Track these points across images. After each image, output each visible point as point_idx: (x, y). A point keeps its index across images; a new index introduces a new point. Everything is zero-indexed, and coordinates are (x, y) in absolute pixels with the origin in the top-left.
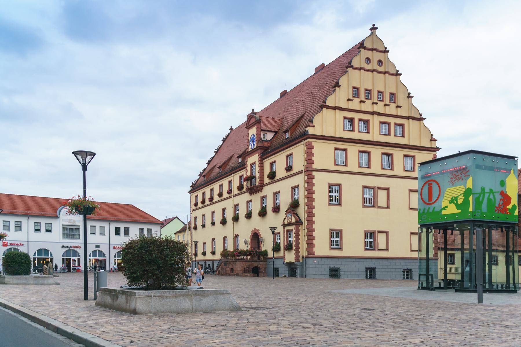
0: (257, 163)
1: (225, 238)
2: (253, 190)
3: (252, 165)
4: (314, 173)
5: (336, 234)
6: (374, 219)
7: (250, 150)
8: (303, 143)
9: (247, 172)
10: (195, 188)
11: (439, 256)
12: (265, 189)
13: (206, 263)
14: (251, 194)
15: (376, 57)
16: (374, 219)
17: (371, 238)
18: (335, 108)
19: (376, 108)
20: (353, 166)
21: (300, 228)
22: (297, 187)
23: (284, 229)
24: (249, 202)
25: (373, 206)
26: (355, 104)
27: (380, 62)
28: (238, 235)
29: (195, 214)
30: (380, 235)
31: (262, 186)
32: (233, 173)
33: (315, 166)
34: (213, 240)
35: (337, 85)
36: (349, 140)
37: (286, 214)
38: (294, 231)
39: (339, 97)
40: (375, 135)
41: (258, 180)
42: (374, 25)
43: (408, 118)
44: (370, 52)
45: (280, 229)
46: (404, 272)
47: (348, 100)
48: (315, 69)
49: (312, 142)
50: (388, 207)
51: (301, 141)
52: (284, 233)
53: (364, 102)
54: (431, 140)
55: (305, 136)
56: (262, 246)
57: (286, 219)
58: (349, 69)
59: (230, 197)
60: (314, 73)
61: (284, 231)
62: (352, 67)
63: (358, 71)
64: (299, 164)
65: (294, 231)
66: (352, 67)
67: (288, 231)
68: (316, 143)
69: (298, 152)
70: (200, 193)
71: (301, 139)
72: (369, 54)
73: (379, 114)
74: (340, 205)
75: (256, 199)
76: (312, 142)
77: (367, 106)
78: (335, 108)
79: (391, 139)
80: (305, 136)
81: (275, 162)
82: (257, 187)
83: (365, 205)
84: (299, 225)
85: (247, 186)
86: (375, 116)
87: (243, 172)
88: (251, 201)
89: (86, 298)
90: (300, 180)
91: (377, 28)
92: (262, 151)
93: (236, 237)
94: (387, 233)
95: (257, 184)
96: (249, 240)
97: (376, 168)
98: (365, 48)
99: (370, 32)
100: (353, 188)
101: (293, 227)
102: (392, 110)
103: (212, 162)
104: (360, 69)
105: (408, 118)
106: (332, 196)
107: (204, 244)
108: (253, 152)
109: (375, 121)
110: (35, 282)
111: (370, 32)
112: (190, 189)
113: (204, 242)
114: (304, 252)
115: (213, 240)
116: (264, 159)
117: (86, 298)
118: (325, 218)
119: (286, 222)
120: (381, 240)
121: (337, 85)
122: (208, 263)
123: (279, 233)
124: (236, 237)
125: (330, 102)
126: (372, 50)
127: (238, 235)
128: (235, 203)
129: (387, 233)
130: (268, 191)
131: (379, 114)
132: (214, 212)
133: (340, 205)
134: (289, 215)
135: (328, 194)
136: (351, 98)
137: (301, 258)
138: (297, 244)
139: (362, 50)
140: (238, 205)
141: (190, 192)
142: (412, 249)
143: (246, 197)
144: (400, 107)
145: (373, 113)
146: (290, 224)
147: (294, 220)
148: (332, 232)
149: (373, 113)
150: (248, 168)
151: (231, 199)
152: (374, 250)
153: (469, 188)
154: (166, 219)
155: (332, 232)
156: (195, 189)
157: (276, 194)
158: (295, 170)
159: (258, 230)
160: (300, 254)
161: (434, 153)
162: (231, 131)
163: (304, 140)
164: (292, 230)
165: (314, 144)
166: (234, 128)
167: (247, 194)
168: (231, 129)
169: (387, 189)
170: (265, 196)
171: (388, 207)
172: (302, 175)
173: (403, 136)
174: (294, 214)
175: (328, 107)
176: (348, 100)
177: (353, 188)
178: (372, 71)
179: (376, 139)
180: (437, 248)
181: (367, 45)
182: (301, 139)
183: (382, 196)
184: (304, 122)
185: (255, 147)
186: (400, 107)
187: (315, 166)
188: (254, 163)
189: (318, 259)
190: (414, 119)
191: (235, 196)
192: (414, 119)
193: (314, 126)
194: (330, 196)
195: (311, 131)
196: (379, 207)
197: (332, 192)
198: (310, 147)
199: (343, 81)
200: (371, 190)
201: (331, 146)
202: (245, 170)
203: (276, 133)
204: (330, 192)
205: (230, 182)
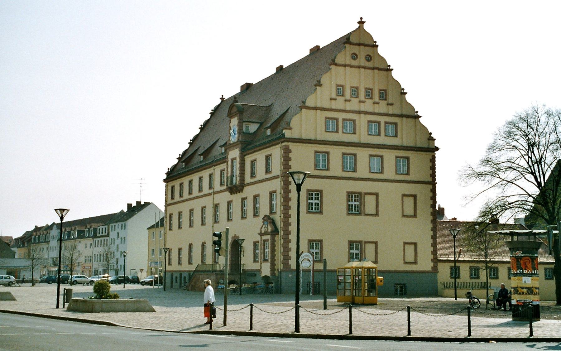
2: (234, 189)
3: (233, 160)
5: (316, 244)
6: (361, 228)
10: (172, 175)
12: (246, 189)
13: (181, 275)
15: (362, 52)
16: (361, 228)
17: (357, 248)
18: (316, 108)
19: (363, 108)
20: (336, 168)
21: (276, 238)
22: (275, 192)
24: (229, 203)
25: (360, 214)
26: (339, 104)
27: (369, 58)
30: (368, 245)
34: (190, 246)
35: (319, 84)
38: (270, 241)
39: (321, 97)
40: (363, 136)
41: (238, 179)
42: (361, 18)
43: (401, 116)
44: (357, 47)
47: (331, 99)
48: (311, 50)
49: (288, 146)
50: (377, 214)
53: (350, 101)
54: (429, 139)
55: (282, 138)
57: (263, 228)
58: (333, 67)
60: (309, 53)
63: (342, 68)
64: (277, 168)
66: (336, 65)
68: (292, 146)
69: (276, 152)
70: (177, 183)
71: (277, 142)
72: (356, 49)
73: (366, 113)
74: (321, 212)
75: (236, 198)
76: (288, 146)
77: (354, 105)
78: (316, 108)
79: (382, 140)
80: (282, 138)
84: (275, 235)
86: (362, 115)
89: (58, 307)
90: (277, 185)
91: (364, 22)
92: (244, 146)
94: (376, 243)
97: (363, 171)
98: (351, 44)
99: (358, 25)
100: (335, 195)
101: (268, 237)
103: (218, 112)
104: (345, 66)
105: (401, 116)
106: (312, 203)
107: (180, 250)
108: (234, 145)
109: (362, 121)
111: (358, 25)
112: (165, 177)
114: (279, 266)
115: (190, 246)
117: (58, 307)
118: (311, 227)
119: (263, 232)
120: (370, 250)
121: (319, 84)
125: (310, 102)
126: (359, 45)
130: (249, 192)
131: (366, 113)
133: (321, 212)
135: (307, 201)
136: (334, 96)
137: (276, 272)
138: (273, 256)
139: (347, 46)
141: (165, 181)
143: (227, 196)
144: (392, 104)
145: (359, 112)
146: (266, 234)
149: (359, 112)
153: (110, 287)
156: (170, 177)
160: (276, 267)
161: (433, 154)
162: (222, 101)
163: (282, 142)
164: (267, 240)
166: (226, 97)
167: (227, 193)
168: (222, 99)
169: (377, 195)
170: (246, 198)
171: (377, 214)
172: (279, 179)
173: (396, 136)
175: (308, 108)
176: (331, 99)
177: (335, 195)
178: (359, 67)
179: (363, 141)
181: (352, 40)
182: (277, 142)
183: (370, 202)
184: (283, 124)
186: (392, 104)
188: (235, 158)
190: (408, 117)
191: (215, 193)
192: (408, 117)
193: (291, 129)
195: (288, 134)
196: (366, 215)
197: (355, 205)
198: (287, 151)
199: (325, 80)
202: (225, 164)
203: (261, 124)
204: (309, 199)
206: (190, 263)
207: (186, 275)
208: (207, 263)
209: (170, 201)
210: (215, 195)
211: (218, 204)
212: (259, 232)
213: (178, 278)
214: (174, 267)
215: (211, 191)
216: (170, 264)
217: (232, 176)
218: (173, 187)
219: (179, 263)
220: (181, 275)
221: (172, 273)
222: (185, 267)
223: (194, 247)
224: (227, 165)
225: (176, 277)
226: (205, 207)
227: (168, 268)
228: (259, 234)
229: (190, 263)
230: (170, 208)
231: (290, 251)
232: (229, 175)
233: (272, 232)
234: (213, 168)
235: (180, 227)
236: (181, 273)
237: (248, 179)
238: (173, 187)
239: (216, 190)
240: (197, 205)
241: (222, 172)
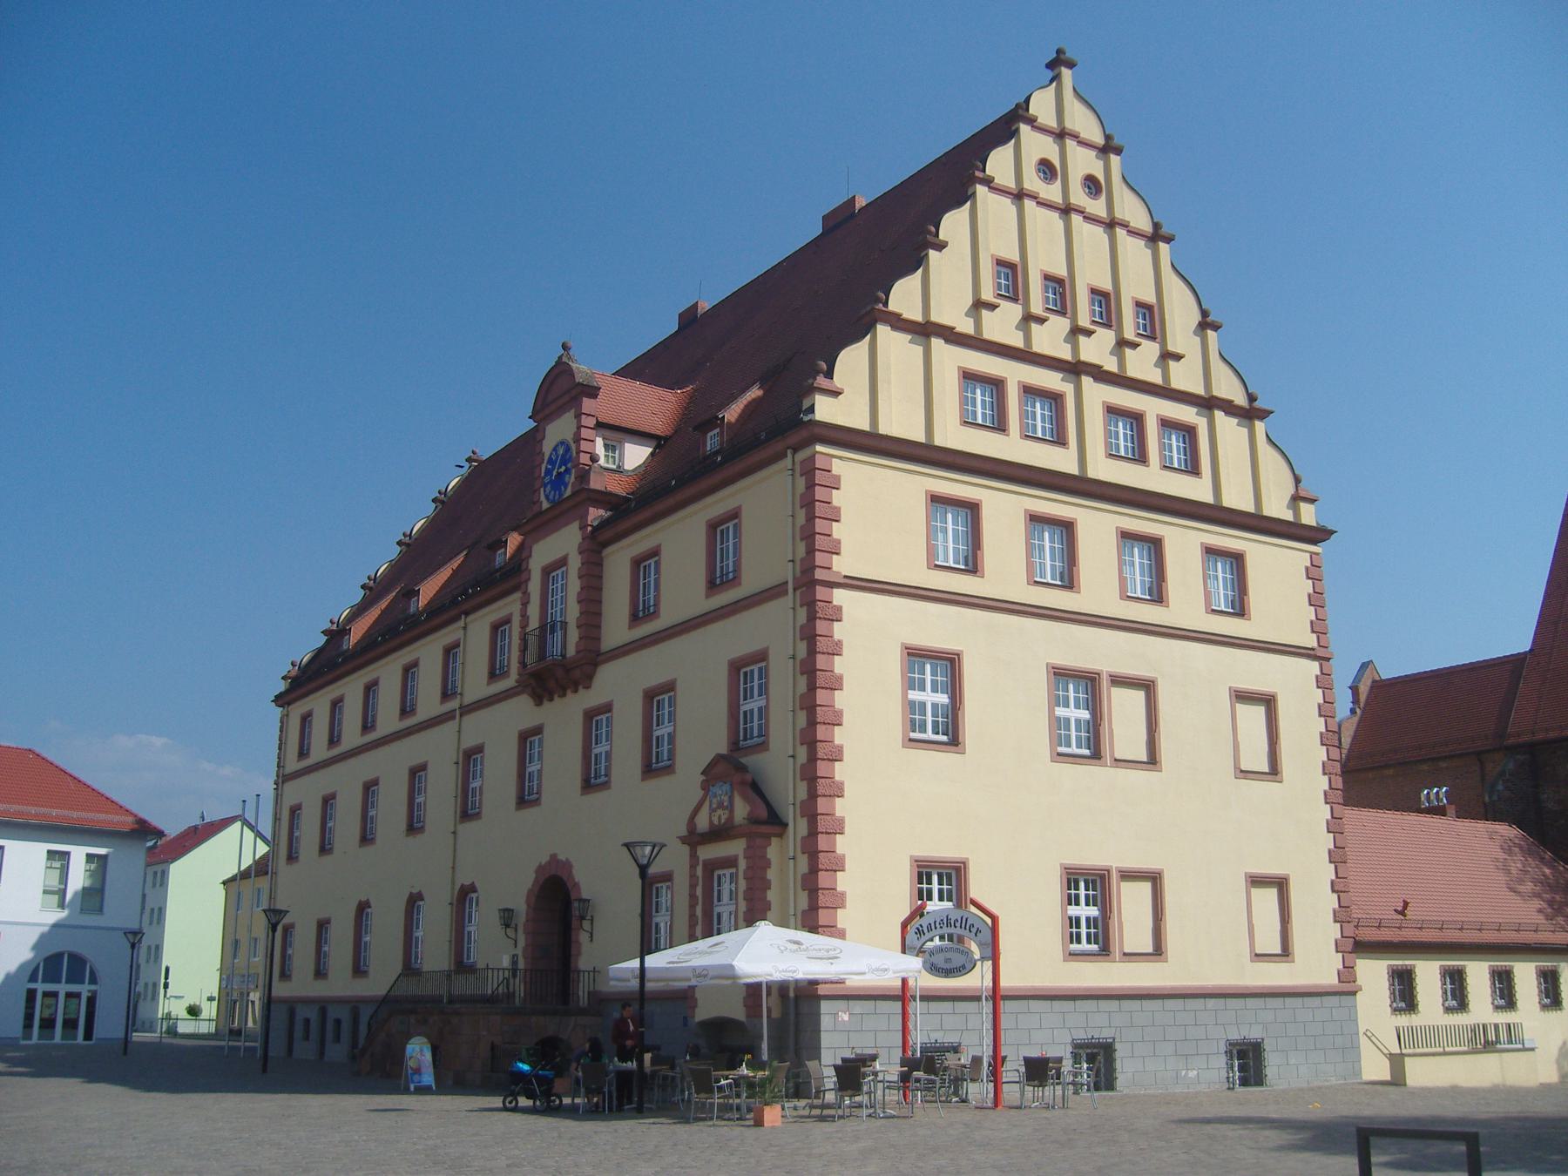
0: (575, 563)
1: (414, 901)
2: (549, 678)
3: (547, 571)
4: (840, 596)
6: (1105, 817)
7: (545, 505)
8: (788, 462)
9: (525, 604)
11: (1361, 979)
13: (323, 1012)
14: (539, 701)
21: (773, 852)
22: (762, 656)
23: (693, 856)
24: (528, 738)
25: (1096, 755)
26: (1002, 325)
28: (473, 888)
29: (293, 793)
31: (592, 658)
32: (467, 614)
33: (843, 565)
34: (363, 908)
36: (988, 467)
37: (706, 786)
38: (742, 864)
39: (944, 284)
41: (573, 635)
45: (674, 860)
46: (1229, 1054)
50: (1153, 760)
51: (783, 456)
52: (693, 876)
56: (583, 937)
57: (705, 810)
59: (447, 717)
61: (693, 867)
62: (1031, 121)
65: (742, 864)
67: (712, 866)
70: (319, 704)
75: (562, 719)
77: (1050, 338)
81: (655, 553)
82: (565, 665)
83: (1062, 749)
84: (768, 837)
85: (523, 664)
87: (509, 606)
88: (538, 730)
93: (464, 896)
94: (1155, 879)
95: (571, 651)
96: (520, 905)
100: (1009, 673)
101: (736, 848)
102: (1143, 363)
106: (923, 705)
107: (323, 926)
110: (798, 827)
112: (282, 686)
113: (322, 916)
115: (363, 908)
116: (606, 544)
119: (703, 823)
122: (333, 1013)
123: (667, 877)
124: (464, 896)
127: (473, 888)
128: (469, 742)
129: (1155, 879)
130: (618, 684)
132: (375, 782)
134: (721, 790)
140: (479, 749)
141: (280, 700)
142: (1278, 951)
143: (521, 711)
146: (718, 833)
147: (741, 810)
148: (924, 871)
150: (534, 586)
151: (451, 726)
152: (1105, 951)
154: (198, 822)
155: (924, 871)
157: (652, 697)
158: (751, 582)
159: (567, 865)
163: (795, 450)
164: (731, 862)
165: (837, 467)
166: (485, 455)
167: (524, 702)
170: (607, 708)
174: (743, 783)
177: (1009, 673)
180: (1350, 943)
183: (1125, 708)
185: (568, 492)
187: (843, 565)
188: (563, 562)
189: (858, 1007)
191: (467, 710)
193: (836, 393)
194: (912, 704)
195: (825, 410)
196: (1118, 762)
200: (1083, 683)
201: (921, 482)
202: (517, 595)
205: (450, 651)
206: (359, 970)
207: (302, 1013)
208: (425, 969)
209: (293, 765)
210: (466, 718)
211: (479, 749)
212: (683, 831)
213: (314, 1026)
214: (302, 985)
215: (453, 704)
216: (285, 976)
217: (547, 628)
218: (306, 719)
219: (320, 973)
220: (323, 1012)
221: (291, 1005)
222: (342, 984)
223: (374, 911)
224: (526, 594)
225: (337, 1039)
226: (375, 782)
227: (281, 990)
228: (684, 840)
229: (359, 970)
230: (289, 787)
231: (843, 906)
232: (534, 623)
233: (753, 820)
234: (461, 623)
235: (325, 848)
236: (323, 1005)
237: (616, 628)
238: (306, 719)
239: (469, 698)
240: (390, 765)
241: (497, 628)
